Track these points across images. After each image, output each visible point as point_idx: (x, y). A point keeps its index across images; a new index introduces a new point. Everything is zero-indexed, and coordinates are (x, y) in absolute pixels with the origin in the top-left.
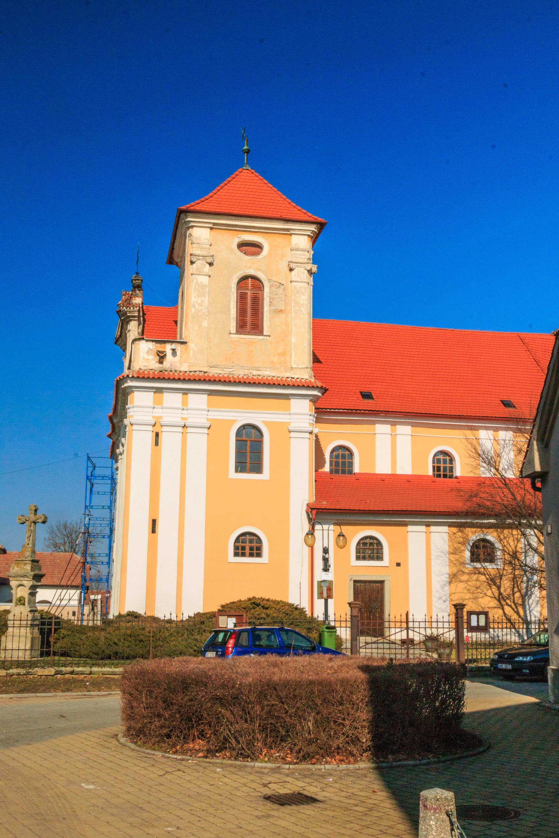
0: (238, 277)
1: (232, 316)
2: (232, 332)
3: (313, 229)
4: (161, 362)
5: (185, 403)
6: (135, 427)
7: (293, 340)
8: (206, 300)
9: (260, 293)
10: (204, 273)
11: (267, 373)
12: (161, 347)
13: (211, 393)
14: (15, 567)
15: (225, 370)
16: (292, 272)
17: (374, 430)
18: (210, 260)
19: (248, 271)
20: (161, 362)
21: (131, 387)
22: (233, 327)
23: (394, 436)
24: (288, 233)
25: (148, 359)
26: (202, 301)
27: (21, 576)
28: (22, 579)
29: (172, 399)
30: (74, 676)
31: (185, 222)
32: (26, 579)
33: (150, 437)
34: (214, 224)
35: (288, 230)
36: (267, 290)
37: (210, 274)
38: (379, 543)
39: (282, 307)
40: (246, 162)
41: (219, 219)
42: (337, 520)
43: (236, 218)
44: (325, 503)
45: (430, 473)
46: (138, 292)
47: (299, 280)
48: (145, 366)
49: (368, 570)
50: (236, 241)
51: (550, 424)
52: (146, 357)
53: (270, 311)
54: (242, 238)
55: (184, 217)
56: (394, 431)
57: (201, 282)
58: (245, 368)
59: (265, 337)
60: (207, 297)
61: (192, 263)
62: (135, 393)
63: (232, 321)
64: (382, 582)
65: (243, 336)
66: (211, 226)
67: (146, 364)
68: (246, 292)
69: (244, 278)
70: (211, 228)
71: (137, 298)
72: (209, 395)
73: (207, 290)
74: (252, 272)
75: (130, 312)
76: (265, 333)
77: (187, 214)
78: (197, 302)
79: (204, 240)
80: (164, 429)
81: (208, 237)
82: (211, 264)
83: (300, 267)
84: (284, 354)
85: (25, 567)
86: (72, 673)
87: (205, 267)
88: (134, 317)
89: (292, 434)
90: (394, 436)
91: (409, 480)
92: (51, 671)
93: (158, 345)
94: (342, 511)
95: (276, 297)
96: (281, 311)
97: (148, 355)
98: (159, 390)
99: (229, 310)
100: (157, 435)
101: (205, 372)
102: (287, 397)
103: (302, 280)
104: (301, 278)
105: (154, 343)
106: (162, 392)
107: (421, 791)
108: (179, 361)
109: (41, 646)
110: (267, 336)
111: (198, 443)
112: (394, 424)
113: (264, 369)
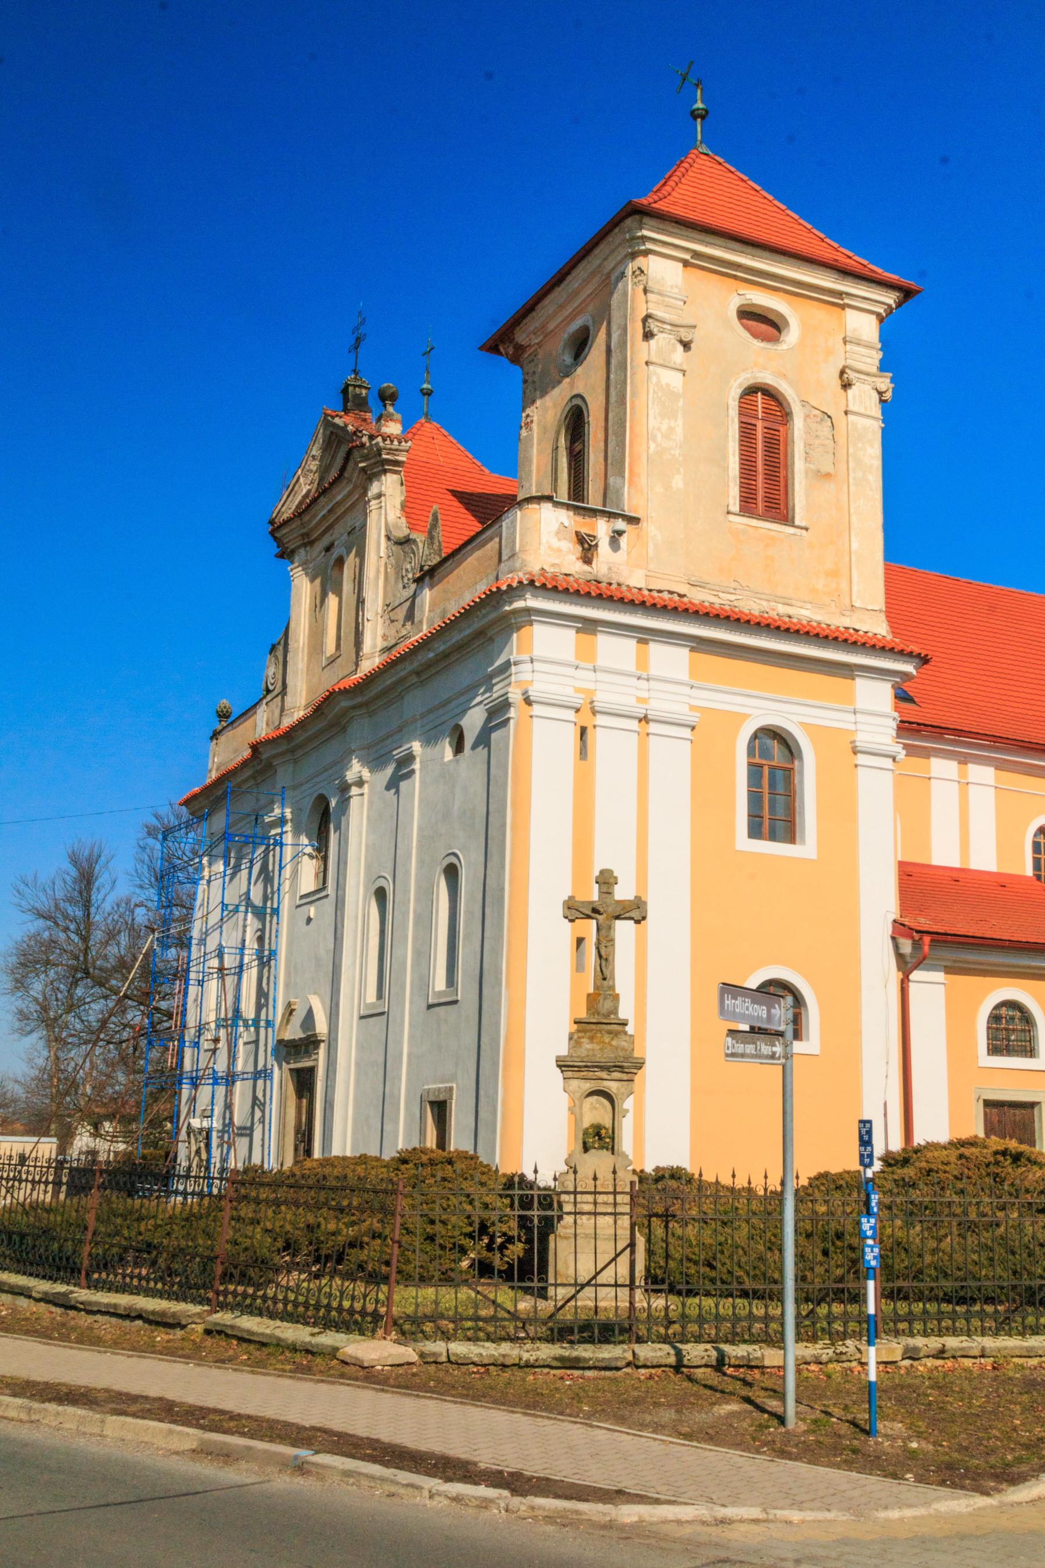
0: (740, 385)
1: (731, 474)
2: (732, 509)
3: (891, 302)
4: (587, 560)
5: (642, 662)
6: (537, 710)
7: (855, 545)
8: (679, 425)
9: (781, 429)
10: (672, 365)
11: (805, 613)
12: (584, 524)
13: (700, 645)
15: (721, 595)
16: (850, 392)
17: (928, 769)
18: (686, 336)
19: (761, 375)
20: (587, 560)
21: (528, 611)
22: (734, 497)
23: (964, 785)
24: (838, 302)
25: (559, 550)
26: (671, 429)
27: (602, 1068)
28: (604, 1074)
29: (615, 650)
30: (949, 1363)
31: (633, 238)
32: (617, 1075)
33: (571, 734)
34: (696, 254)
35: (840, 294)
36: (798, 423)
37: (685, 367)
38: (1027, 1018)
39: (828, 468)
40: (699, 137)
41: (708, 244)
42: (955, 961)
43: (744, 248)
44: (922, 920)
45: (1029, 871)
46: (390, 409)
47: (862, 411)
48: (553, 565)
49: (1009, 1077)
50: (735, 303)
52: (555, 543)
53: (807, 472)
54: (748, 297)
55: (635, 225)
56: (963, 774)
57: (668, 385)
58: (763, 596)
59: (798, 531)
60: (680, 422)
61: (648, 335)
62: (537, 628)
63: (731, 484)
64: (1032, 1105)
65: (754, 522)
66: (687, 257)
67: (556, 562)
68: (753, 421)
69: (751, 391)
70: (686, 264)
71: (391, 424)
72: (693, 650)
73: (680, 404)
74: (767, 378)
75: (390, 451)
76: (797, 522)
77: (646, 220)
78: (659, 429)
79: (672, 287)
80: (600, 720)
81: (680, 283)
82: (686, 345)
83: (864, 382)
84: (834, 574)
85: (614, 1043)
86: (940, 1354)
87: (674, 350)
88: (397, 463)
89: (861, 759)
90: (964, 785)
91: (1000, 884)
92: (893, 1350)
93: (579, 519)
94: (972, 940)
95: (817, 442)
96: (828, 475)
97: (559, 540)
98: (589, 626)
99: (725, 458)
100: (583, 731)
101: (680, 595)
102: (848, 671)
103: (868, 413)
104: (866, 408)
105: (571, 513)
106: (594, 633)
108: (620, 565)
110: (802, 528)
111: (672, 758)
112: (964, 760)
113: (800, 604)
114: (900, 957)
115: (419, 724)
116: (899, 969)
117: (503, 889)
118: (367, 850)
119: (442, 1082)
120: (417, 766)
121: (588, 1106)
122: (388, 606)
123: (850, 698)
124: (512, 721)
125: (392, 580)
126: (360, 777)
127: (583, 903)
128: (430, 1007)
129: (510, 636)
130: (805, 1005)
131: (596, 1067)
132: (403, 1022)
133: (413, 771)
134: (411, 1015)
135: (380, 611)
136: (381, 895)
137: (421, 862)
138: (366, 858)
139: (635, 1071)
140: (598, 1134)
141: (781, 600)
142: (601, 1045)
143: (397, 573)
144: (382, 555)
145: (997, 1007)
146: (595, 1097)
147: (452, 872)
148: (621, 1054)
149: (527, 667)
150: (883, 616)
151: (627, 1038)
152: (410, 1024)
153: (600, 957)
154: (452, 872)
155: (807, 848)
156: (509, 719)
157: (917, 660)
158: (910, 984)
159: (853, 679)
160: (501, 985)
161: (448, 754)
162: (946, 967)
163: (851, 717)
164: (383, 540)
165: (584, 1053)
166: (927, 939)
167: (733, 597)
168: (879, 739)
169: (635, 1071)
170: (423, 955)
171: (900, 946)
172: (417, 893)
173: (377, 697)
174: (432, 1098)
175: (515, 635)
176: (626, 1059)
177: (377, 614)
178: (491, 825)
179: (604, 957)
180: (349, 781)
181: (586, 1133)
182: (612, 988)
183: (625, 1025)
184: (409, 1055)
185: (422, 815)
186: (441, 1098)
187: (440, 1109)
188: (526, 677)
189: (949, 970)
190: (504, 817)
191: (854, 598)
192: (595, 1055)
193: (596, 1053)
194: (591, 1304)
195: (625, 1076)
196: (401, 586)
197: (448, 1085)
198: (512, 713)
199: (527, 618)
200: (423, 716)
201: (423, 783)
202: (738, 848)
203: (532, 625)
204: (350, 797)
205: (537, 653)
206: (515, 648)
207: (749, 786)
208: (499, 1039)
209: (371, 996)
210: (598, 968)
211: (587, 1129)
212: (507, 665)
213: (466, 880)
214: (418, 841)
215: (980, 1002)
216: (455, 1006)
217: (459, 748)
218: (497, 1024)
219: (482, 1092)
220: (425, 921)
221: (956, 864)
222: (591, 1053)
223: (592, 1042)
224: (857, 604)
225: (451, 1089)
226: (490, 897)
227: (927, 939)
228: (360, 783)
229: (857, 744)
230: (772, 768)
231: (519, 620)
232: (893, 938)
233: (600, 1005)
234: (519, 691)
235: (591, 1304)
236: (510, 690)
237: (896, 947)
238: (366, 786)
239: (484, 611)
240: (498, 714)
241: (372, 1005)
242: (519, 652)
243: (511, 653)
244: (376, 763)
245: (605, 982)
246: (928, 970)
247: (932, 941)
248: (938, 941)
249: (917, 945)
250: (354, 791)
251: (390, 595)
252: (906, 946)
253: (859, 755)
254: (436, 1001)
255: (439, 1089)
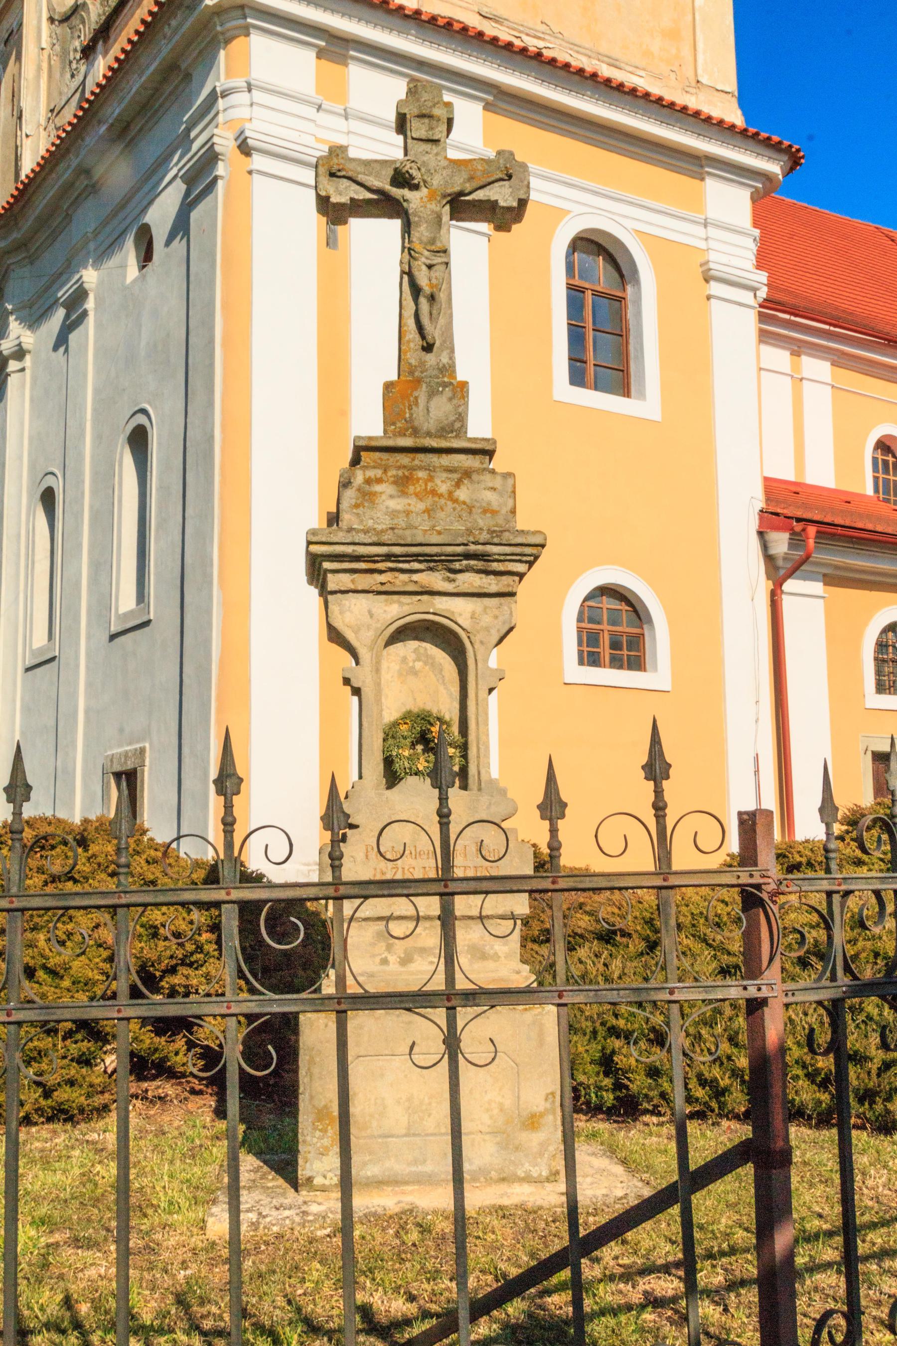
6: (258, 161)
14: (385, 489)
27: (432, 561)
28: (436, 580)
32: (470, 581)
45: (870, 491)
51: (401, 565)
56: (796, 367)
62: (256, 39)
72: (488, 107)
84: (673, 35)
85: (463, 494)
89: (715, 288)
102: (695, 164)
106: (343, 60)
107: (759, 1287)
109: (289, 1055)
112: (797, 349)
114: (769, 559)
115: (92, 246)
116: (769, 577)
117: (211, 438)
118: (30, 444)
119: (130, 744)
120: (90, 304)
121: (395, 667)
122: (52, 111)
123: (698, 203)
124: (220, 183)
125: (57, 75)
126: (19, 345)
127: (367, 163)
128: (113, 637)
129: (214, 57)
130: (650, 621)
131: (416, 557)
132: (77, 666)
133: (85, 314)
134: (88, 655)
135: (43, 122)
136: (48, 498)
137: (98, 438)
138: (30, 454)
139: (521, 568)
140: (423, 738)
141: (605, 59)
142: (429, 501)
143: (63, 62)
144: (44, 45)
145: (885, 630)
146: (413, 644)
147: (139, 440)
148: (481, 523)
149: (242, 98)
150: (734, 102)
151: (498, 482)
152: (87, 667)
153: (416, 291)
154: (139, 440)
155: (646, 405)
156: (216, 179)
157: (786, 158)
158: (784, 596)
159: (702, 179)
160: (211, 583)
161: (132, 271)
162: (825, 575)
163: (700, 231)
164: (45, 24)
165: (384, 523)
166: (812, 530)
167: (541, 44)
168: (736, 262)
169: (521, 568)
170: (103, 566)
171: (770, 545)
172: (94, 481)
173: (35, 232)
174: (117, 768)
175: (222, 53)
176: (496, 535)
177: (39, 125)
178: (192, 358)
179: (427, 289)
180: (5, 353)
181: (390, 734)
182: (449, 369)
183: (489, 453)
184: (87, 712)
185: (98, 371)
186: (130, 766)
187: (129, 779)
188: (243, 113)
189: (830, 580)
190: (212, 329)
191: (700, 71)
192: (410, 527)
193: (416, 520)
194: (437, 1200)
195: (492, 584)
196: (68, 76)
197: (138, 746)
198: (221, 169)
199: (240, 22)
200: (96, 233)
201: (99, 326)
202: (556, 398)
203: (248, 35)
204: (8, 375)
205: (258, 74)
206: (223, 72)
207: (569, 318)
208: (210, 665)
209: (40, 639)
210: (411, 323)
211: (395, 724)
212: (213, 97)
213: (159, 444)
214: (94, 410)
215: (866, 624)
216: (146, 629)
217: (146, 256)
218: (208, 642)
219: (186, 750)
220: (105, 520)
221: (791, 477)
222: (401, 522)
223: (404, 493)
224: (704, 80)
225: (142, 751)
226: (193, 454)
227: (812, 530)
228: (20, 353)
229: (712, 266)
230: (596, 294)
231: (229, 25)
232: (761, 534)
233: (419, 412)
234: (231, 135)
235: (437, 1200)
236: (216, 131)
237: (765, 547)
238: (28, 357)
239: (174, 23)
240: (201, 180)
241: (41, 650)
242: (228, 75)
243: (218, 79)
244: (34, 319)
245: (430, 359)
246: (805, 579)
247: (818, 532)
248: (824, 533)
249: (797, 539)
250: (13, 365)
251: (55, 94)
252: (780, 542)
253: (712, 283)
254: (120, 629)
255: (126, 754)
